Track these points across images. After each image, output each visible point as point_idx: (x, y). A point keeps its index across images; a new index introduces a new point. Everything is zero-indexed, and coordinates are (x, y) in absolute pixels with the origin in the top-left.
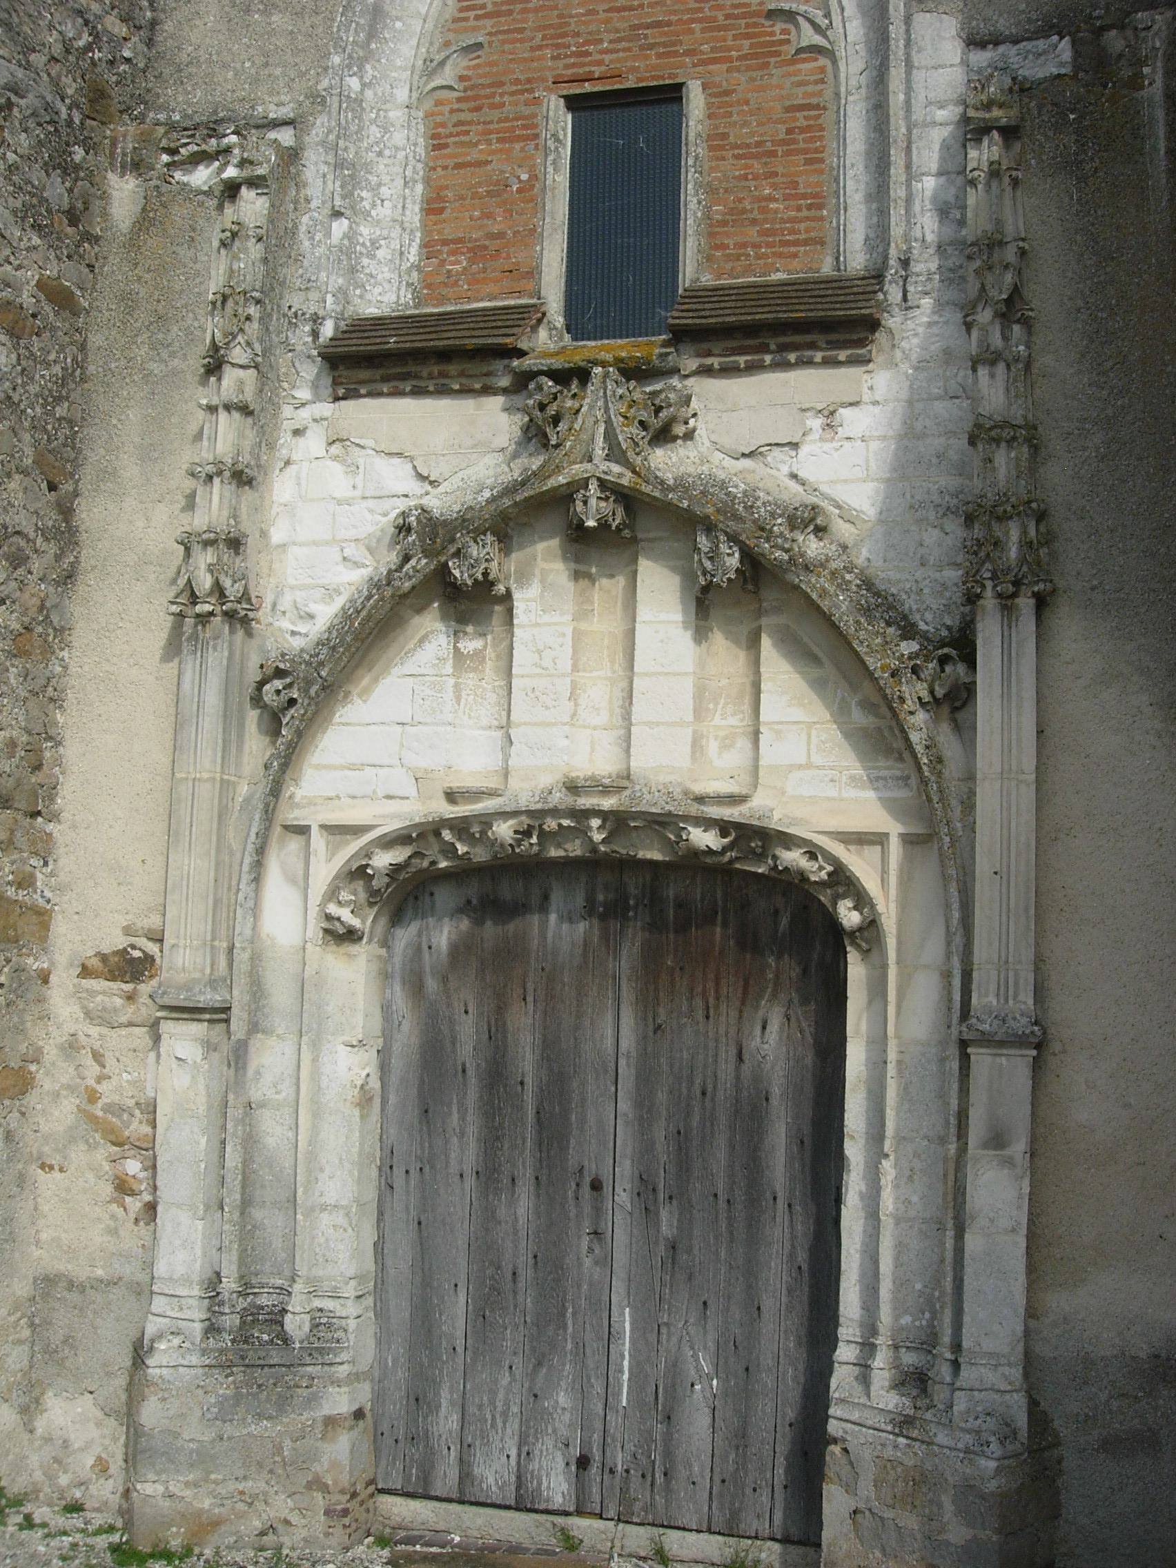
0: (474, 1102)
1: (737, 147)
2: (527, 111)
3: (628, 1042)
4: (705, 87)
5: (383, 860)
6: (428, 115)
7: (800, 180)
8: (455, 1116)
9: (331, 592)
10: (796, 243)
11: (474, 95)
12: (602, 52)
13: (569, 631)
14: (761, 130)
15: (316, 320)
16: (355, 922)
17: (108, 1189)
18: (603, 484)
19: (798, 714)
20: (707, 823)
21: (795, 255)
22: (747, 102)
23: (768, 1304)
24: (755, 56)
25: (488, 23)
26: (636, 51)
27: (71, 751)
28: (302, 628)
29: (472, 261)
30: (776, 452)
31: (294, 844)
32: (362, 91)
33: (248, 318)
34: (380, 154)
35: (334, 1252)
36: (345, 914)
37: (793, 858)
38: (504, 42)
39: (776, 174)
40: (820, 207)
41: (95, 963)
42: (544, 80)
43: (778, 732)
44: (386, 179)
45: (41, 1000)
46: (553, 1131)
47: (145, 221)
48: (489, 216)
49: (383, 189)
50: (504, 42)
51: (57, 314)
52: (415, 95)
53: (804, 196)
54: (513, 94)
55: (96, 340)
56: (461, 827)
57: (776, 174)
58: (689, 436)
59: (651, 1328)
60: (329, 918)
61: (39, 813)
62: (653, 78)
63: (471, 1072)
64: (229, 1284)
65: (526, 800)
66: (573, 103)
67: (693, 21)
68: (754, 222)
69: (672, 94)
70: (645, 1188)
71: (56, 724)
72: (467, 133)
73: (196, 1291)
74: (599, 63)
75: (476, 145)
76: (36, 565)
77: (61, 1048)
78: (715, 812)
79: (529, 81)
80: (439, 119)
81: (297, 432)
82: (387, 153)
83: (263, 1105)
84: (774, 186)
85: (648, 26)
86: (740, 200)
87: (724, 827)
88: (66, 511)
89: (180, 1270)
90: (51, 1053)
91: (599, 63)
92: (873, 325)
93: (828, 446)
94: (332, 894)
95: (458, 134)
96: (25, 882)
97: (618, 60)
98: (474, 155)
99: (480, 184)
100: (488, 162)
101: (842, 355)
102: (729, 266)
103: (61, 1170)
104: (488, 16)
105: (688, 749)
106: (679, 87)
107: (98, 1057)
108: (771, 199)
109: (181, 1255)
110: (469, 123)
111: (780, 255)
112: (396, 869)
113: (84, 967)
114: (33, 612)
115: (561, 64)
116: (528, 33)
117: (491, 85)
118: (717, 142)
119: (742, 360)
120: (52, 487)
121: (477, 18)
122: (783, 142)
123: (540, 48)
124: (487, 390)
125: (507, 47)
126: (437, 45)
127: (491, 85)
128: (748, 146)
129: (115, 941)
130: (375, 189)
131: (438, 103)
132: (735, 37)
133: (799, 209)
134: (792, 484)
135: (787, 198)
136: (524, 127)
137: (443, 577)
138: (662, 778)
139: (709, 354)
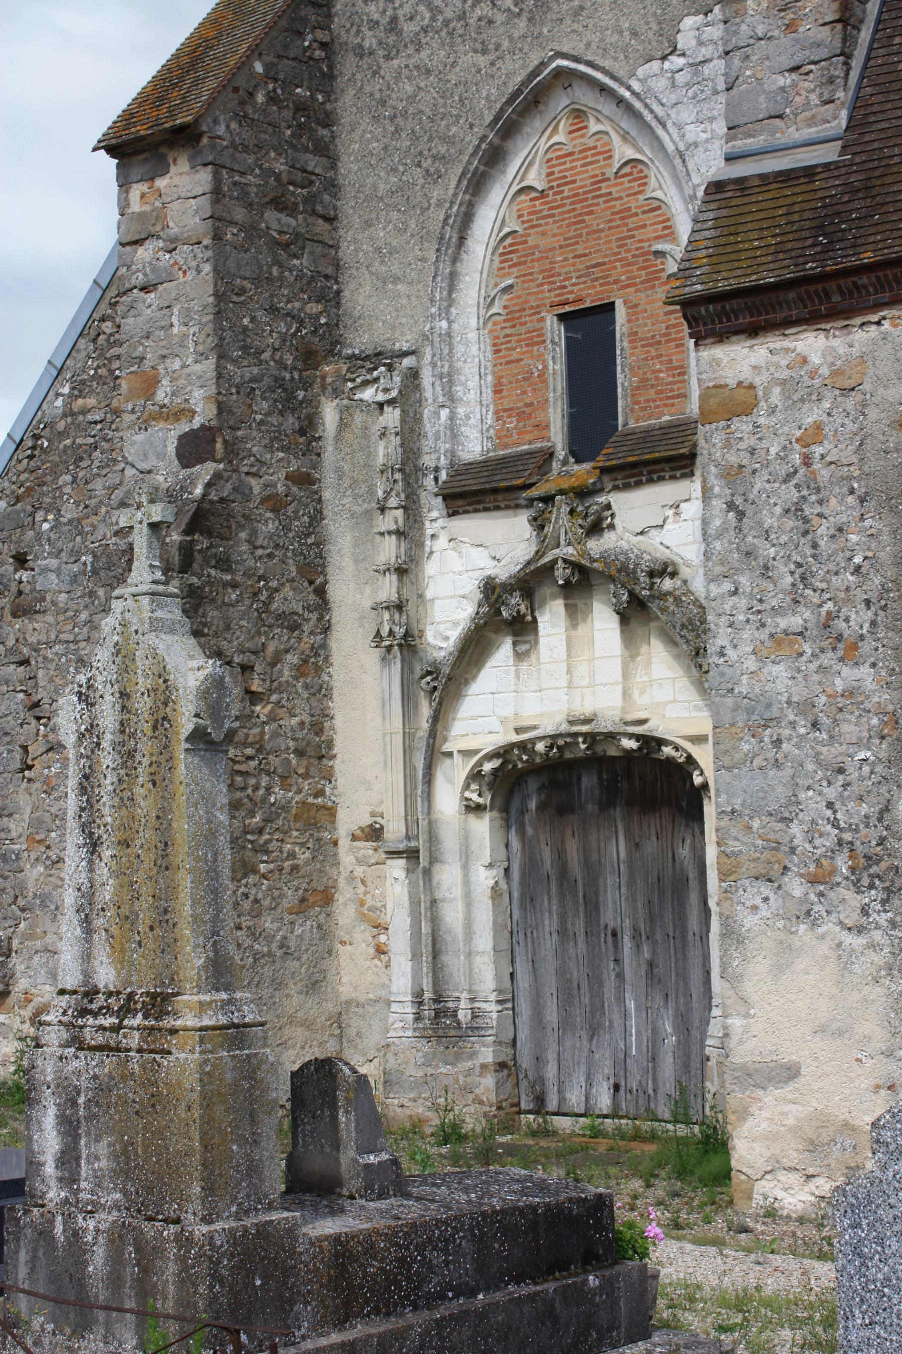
0: (538, 890)
1: (642, 339)
2: (538, 326)
3: (623, 855)
4: (625, 302)
5: (488, 767)
6: (491, 331)
7: (674, 358)
8: (546, 903)
9: (456, 624)
10: (673, 397)
11: (513, 317)
12: (574, 285)
13: (564, 637)
14: (654, 328)
15: (437, 469)
16: (480, 800)
17: (372, 951)
18: (565, 561)
19: (670, 674)
20: (631, 736)
21: (673, 405)
22: (646, 311)
23: (694, 991)
24: (648, 281)
25: (515, 269)
26: (589, 283)
27: (338, 722)
28: (444, 645)
29: (518, 421)
30: (653, 531)
31: (448, 762)
32: (449, 327)
33: (395, 481)
34: (465, 361)
35: (479, 974)
36: (474, 797)
37: (667, 751)
38: (524, 282)
39: (661, 355)
40: (684, 374)
41: (358, 832)
42: (545, 305)
43: (660, 684)
44: (470, 376)
45: (336, 855)
46: (593, 907)
47: (343, 426)
48: (524, 393)
49: (469, 383)
50: (524, 282)
51: (300, 489)
52: (481, 321)
53: (676, 368)
54: (530, 315)
55: (327, 495)
56: (522, 746)
57: (661, 355)
58: (612, 527)
59: (645, 1009)
60: (467, 799)
61: (323, 756)
62: (600, 299)
63: (553, 877)
64: (428, 995)
65: (550, 730)
66: (562, 317)
67: (616, 261)
68: (653, 386)
69: (610, 307)
70: (636, 936)
71: (329, 708)
72: (510, 342)
73: (409, 998)
74: (572, 292)
75: (515, 349)
76: (306, 628)
77: (346, 878)
78: (632, 729)
79: (538, 306)
80: (495, 334)
81: (433, 536)
82: (469, 360)
83: (443, 901)
84: (661, 363)
85: (594, 266)
86: (645, 373)
87: (638, 737)
88: (321, 592)
89: (402, 989)
90: (342, 882)
91: (572, 292)
92: (692, 457)
93: (677, 526)
94: (467, 787)
95: (506, 343)
96: (320, 793)
97: (581, 290)
98: (515, 356)
99: (519, 374)
100: (522, 360)
101: (678, 474)
102: (642, 414)
103: (350, 944)
104: (515, 265)
105: (621, 696)
106: (613, 303)
107: (363, 882)
108: (660, 371)
109: (402, 980)
110: (511, 335)
111: (665, 405)
112: (495, 771)
113: (353, 835)
114: (307, 652)
115: (553, 294)
116: (535, 276)
117: (519, 311)
118: (633, 335)
119: (632, 480)
120: (311, 583)
121: (510, 267)
122: (666, 335)
123: (542, 285)
124: (517, 506)
125: (526, 285)
126: (491, 286)
127: (519, 311)
128: (648, 339)
129: (366, 820)
130: (464, 384)
131: (495, 324)
132: (638, 269)
133: (674, 376)
134: (661, 547)
135: (668, 369)
136: (538, 336)
137: (506, 613)
138: (610, 713)
139: (616, 479)
